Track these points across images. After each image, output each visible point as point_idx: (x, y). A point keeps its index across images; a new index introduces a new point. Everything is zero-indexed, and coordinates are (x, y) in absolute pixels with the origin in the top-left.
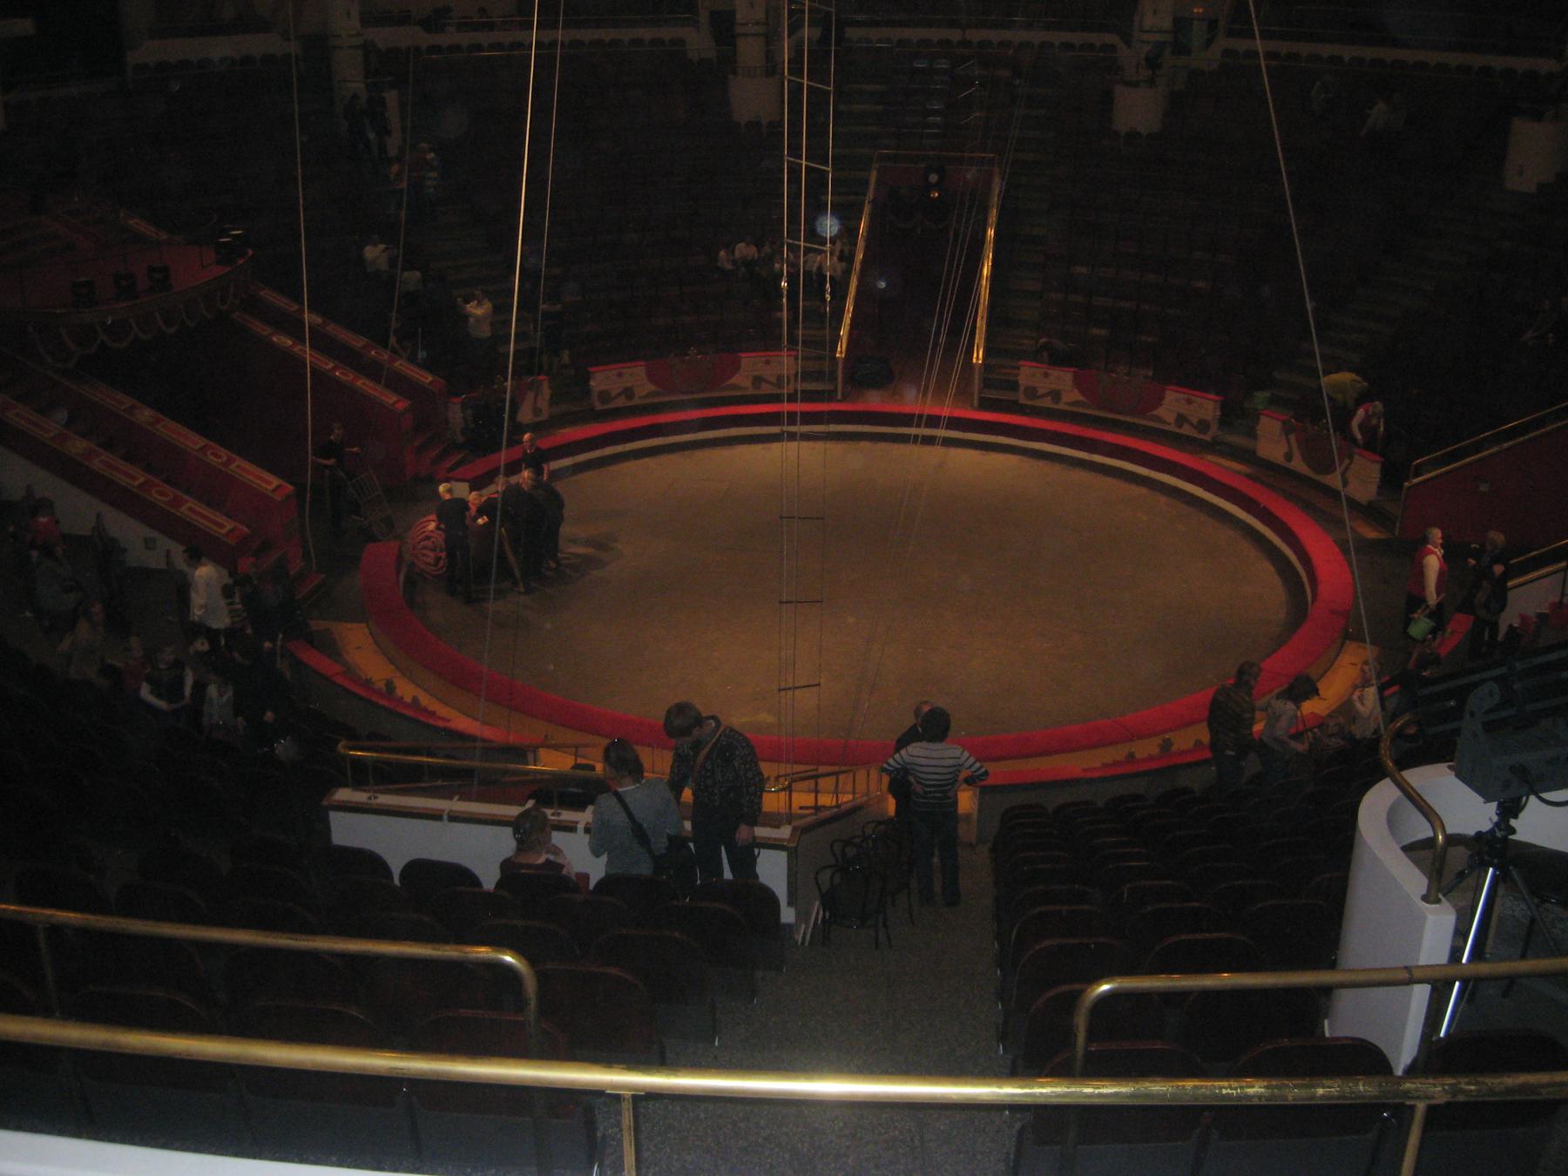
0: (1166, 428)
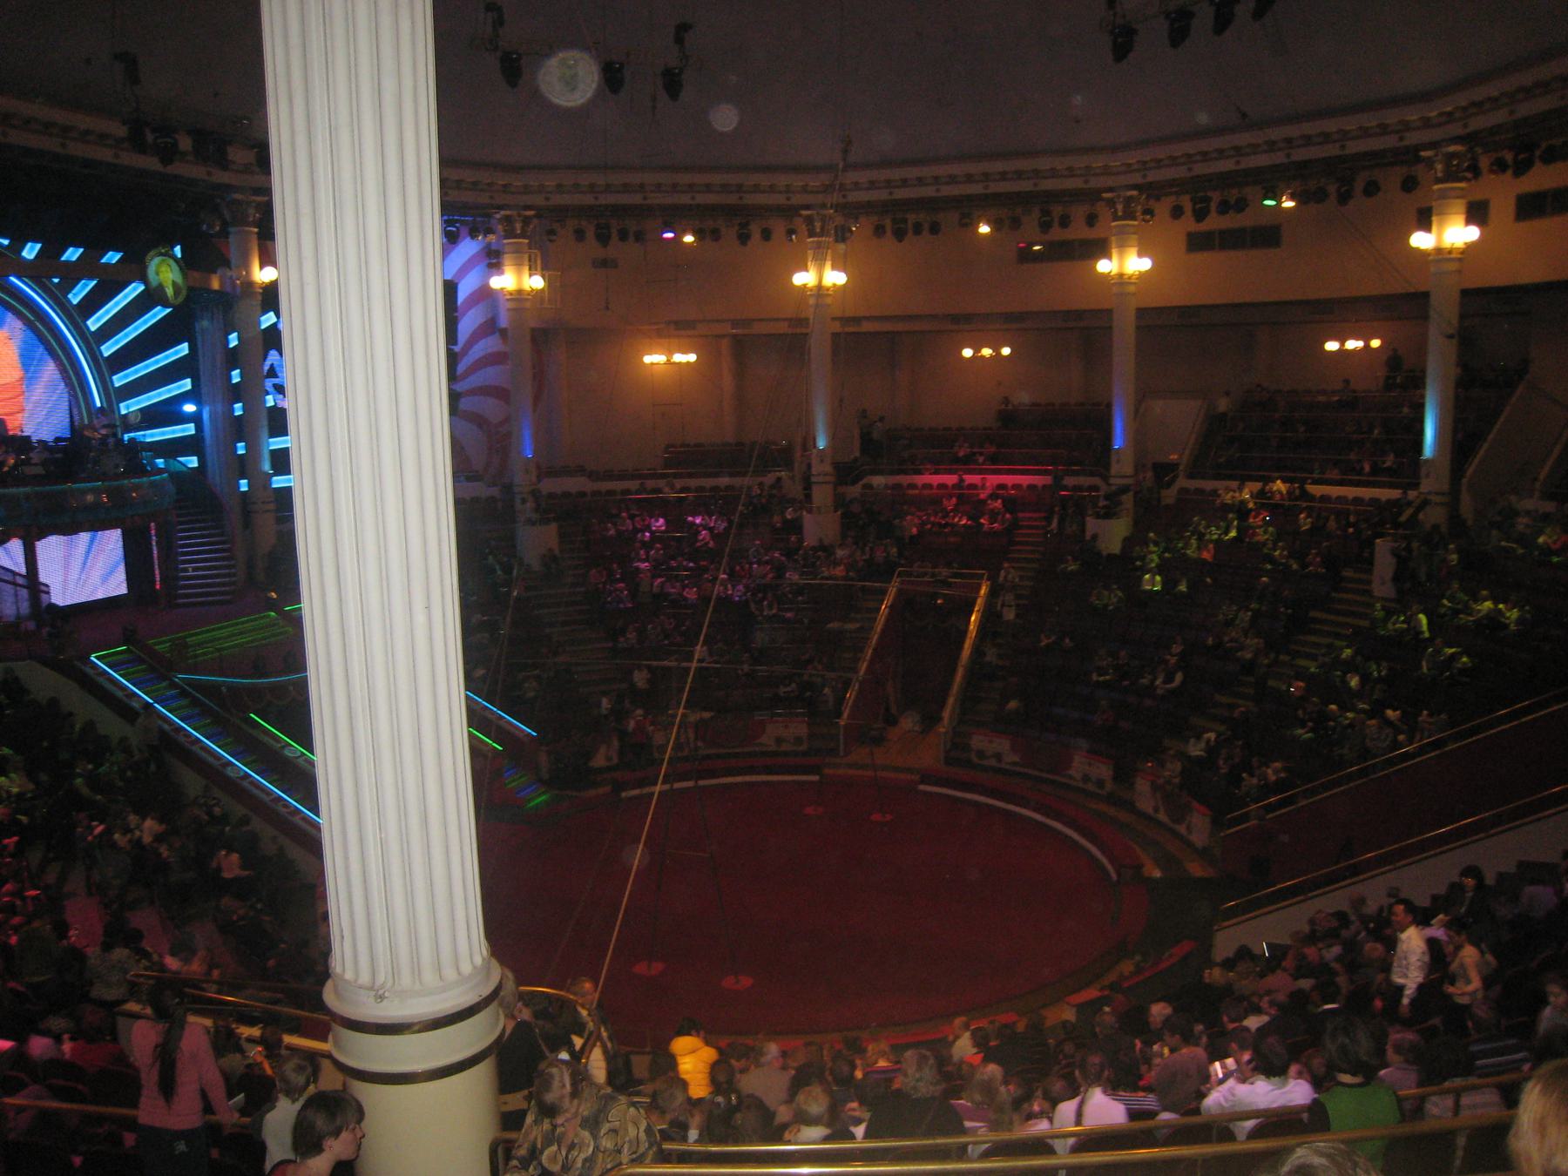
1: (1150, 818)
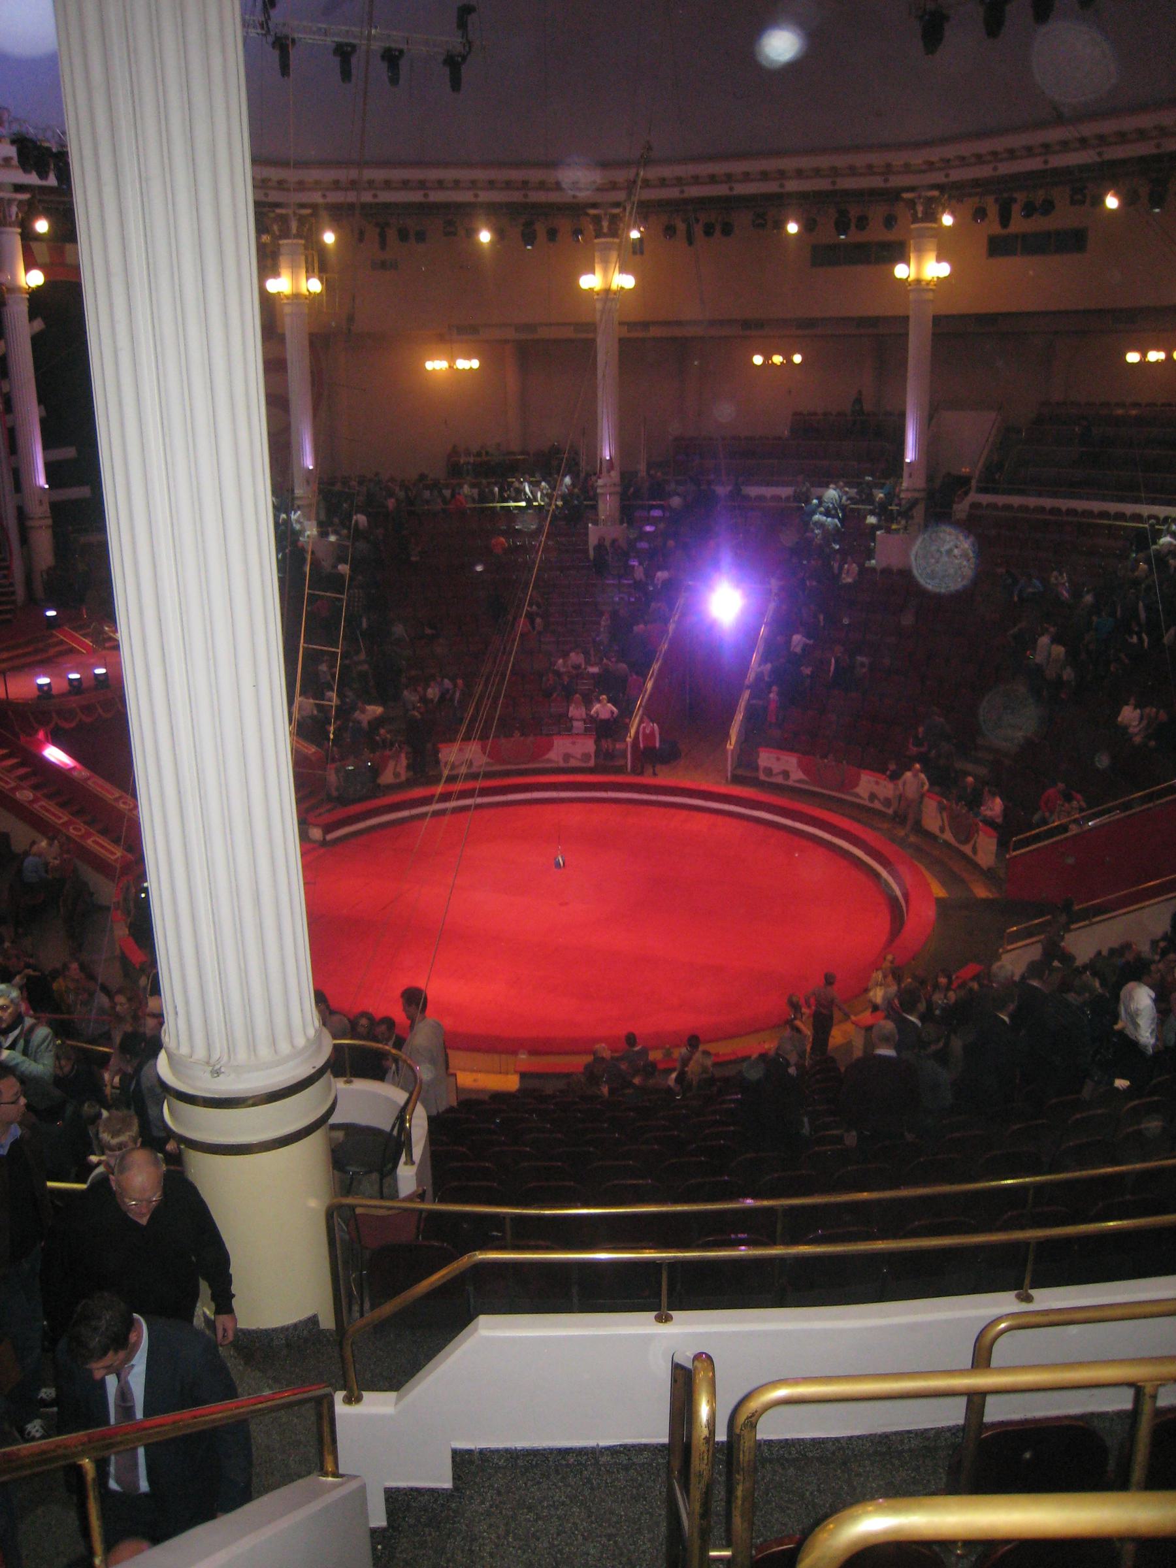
0: (862, 802)
1: (934, 838)
